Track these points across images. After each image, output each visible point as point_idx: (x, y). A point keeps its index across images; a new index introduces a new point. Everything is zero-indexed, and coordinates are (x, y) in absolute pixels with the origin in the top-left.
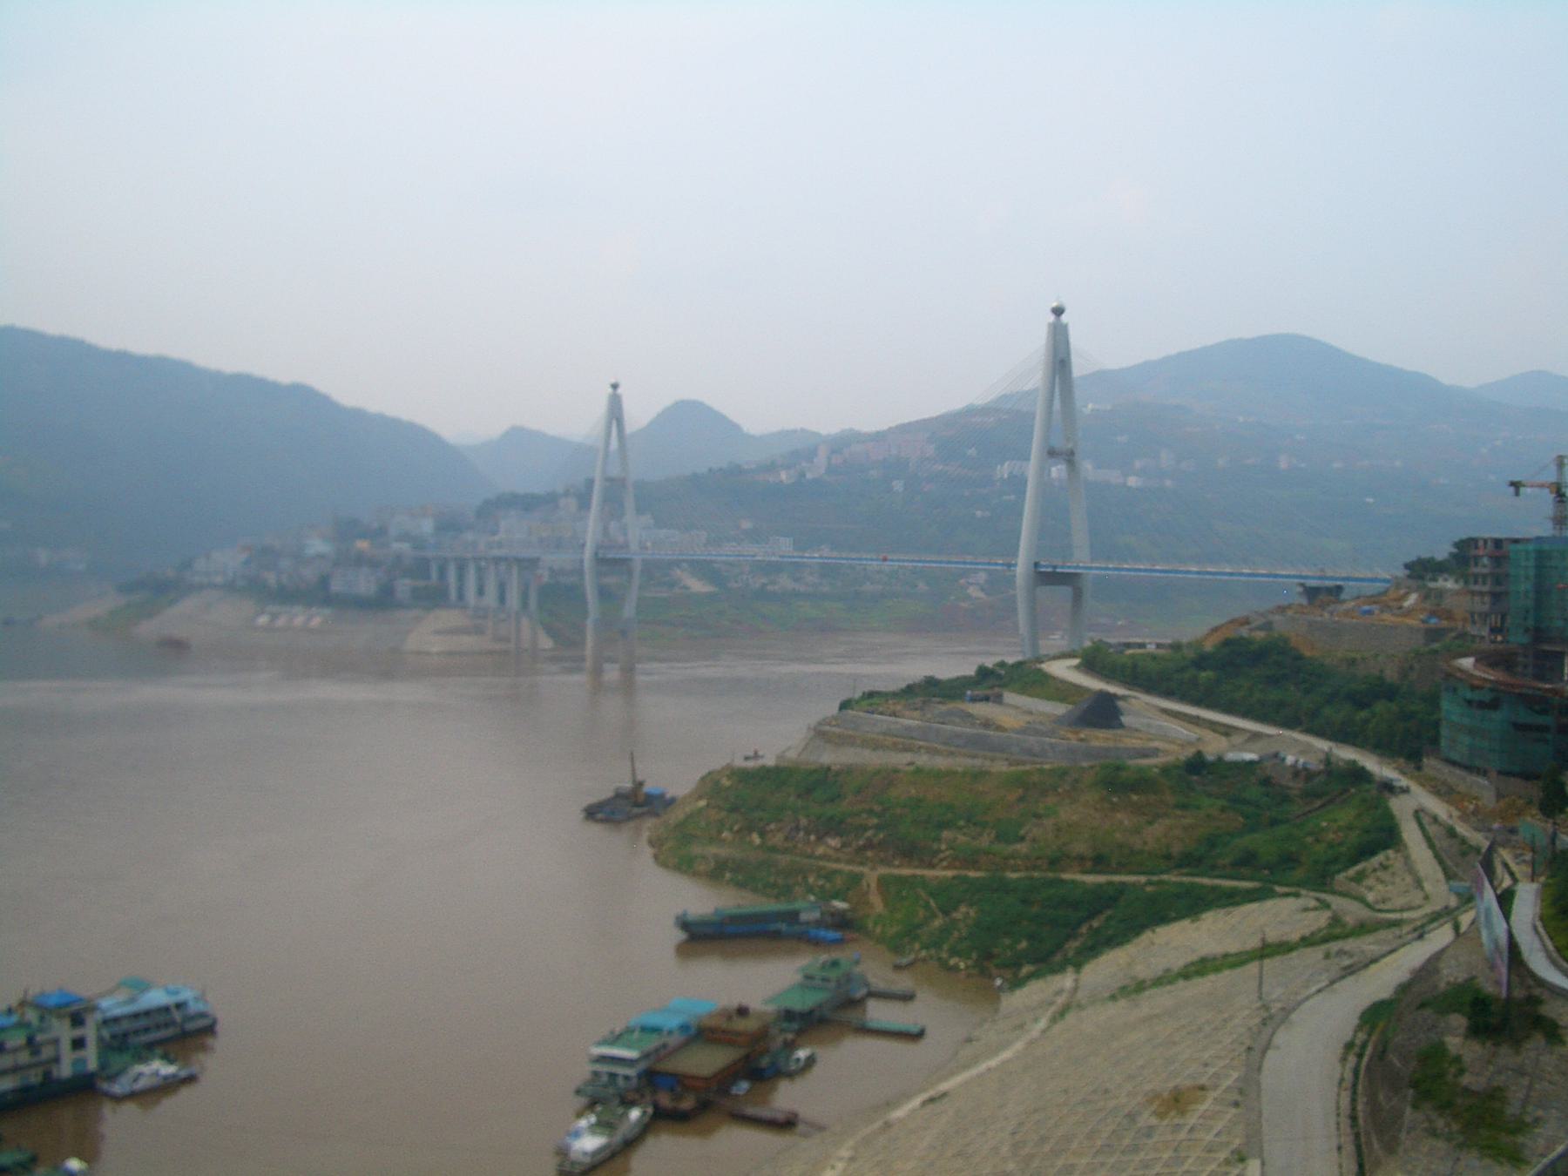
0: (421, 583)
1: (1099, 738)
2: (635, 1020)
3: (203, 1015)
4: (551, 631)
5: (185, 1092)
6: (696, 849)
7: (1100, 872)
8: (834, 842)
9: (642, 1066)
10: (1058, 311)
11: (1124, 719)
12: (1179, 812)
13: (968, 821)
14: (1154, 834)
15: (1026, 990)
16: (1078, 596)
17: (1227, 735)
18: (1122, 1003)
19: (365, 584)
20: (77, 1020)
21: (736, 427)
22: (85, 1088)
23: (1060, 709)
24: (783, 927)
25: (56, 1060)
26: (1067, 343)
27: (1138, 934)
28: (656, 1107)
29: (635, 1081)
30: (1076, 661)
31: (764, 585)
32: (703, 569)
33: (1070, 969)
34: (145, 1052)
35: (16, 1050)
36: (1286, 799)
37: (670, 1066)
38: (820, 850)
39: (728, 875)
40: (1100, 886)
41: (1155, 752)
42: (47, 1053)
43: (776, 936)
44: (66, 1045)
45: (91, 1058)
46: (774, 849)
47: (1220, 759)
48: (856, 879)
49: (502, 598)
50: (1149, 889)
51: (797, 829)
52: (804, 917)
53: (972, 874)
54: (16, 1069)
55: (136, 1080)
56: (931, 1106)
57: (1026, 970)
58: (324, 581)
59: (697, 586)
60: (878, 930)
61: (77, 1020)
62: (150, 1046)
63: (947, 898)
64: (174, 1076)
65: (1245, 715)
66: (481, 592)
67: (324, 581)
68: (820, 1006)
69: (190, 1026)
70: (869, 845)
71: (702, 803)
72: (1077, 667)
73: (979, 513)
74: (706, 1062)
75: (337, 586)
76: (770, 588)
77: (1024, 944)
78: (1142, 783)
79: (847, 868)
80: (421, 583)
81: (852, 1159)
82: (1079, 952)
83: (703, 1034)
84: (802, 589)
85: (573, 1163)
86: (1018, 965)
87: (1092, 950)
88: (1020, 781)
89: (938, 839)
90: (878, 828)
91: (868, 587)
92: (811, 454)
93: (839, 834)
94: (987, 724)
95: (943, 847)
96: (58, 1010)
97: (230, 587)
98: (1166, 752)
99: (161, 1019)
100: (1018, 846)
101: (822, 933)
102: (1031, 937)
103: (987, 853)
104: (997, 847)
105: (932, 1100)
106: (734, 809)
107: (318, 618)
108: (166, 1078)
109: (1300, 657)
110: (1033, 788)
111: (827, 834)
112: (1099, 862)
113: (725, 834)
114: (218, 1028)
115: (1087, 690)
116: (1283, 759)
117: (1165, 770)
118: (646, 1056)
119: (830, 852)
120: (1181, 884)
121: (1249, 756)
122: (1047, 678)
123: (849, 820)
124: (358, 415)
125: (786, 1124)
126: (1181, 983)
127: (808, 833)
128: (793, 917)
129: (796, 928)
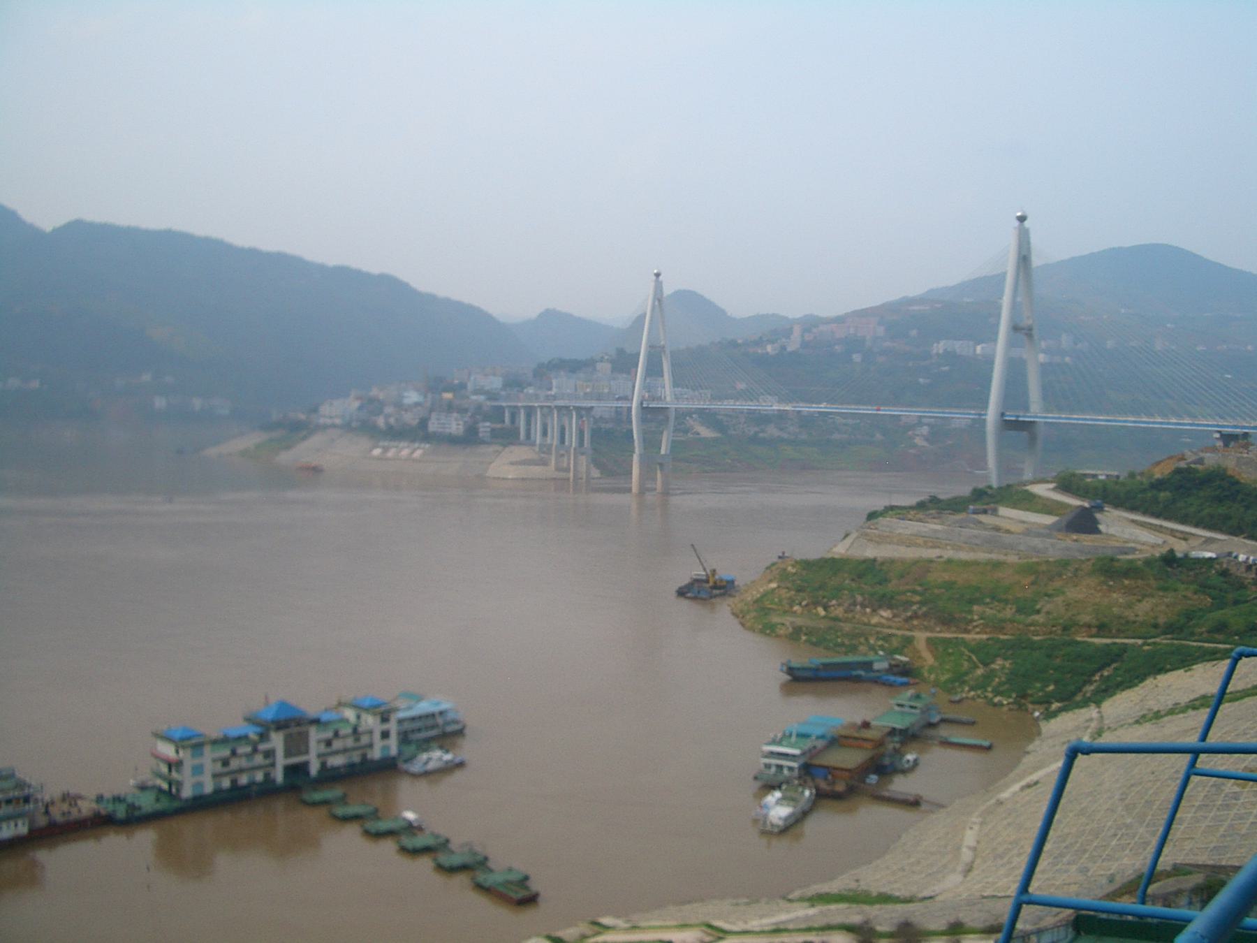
0: (499, 426)
1: (1087, 540)
2: (795, 728)
3: (456, 722)
4: (597, 463)
5: (458, 776)
6: (775, 619)
7: (1102, 637)
8: (886, 613)
9: (802, 761)
10: (1022, 219)
11: (1101, 527)
12: (1161, 593)
13: (993, 598)
14: (1144, 609)
15: (1059, 719)
16: (1033, 439)
17: (1185, 539)
18: (1148, 725)
19: (455, 426)
20: (385, 719)
21: (723, 312)
22: (389, 767)
23: (1049, 520)
24: (862, 673)
25: (371, 746)
26: (1029, 243)
27: (1142, 680)
28: (817, 789)
29: (796, 773)
30: (1052, 486)
31: (756, 433)
32: (708, 417)
33: (1093, 706)
34: (425, 744)
35: (345, 737)
36: (1242, 586)
37: (816, 762)
38: (875, 620)
39: (804, 638)
40: (1107, 645)
41: (1134, 550)
42: (365, 740)
43: (858, 679)
44: (377, 735)
45: (393, 745)
46: (836, 619)
47: (1186, 556)
48: (909, 641)
49: (562, 440)
50: (1146, 648)
51: (855, 604)
52: (876, 666)
53: (1002, 637)
54: (345, 751)
55: (426, 763)
56: (1029, 790)
57: (1055, 705)
58: (424, 423)
59: (706, 432)
60: (933, 677)
61: (385, 719)
62: (428, 741)
63: (984, 654)
64: (451, 761)
65: (1196, 526)
66: (545, 433)
67: (424, 423)
68: (913, 725)
69: (449, 729)
70: (915, 616)
71: (774, 585)
72: (1054, 489)
73: (921, 380)
74: (850, 759)
75: (433, 427)
76: (761, 435)
77: (1051, 688)
78: (1131, 571)
79: (900, 633)
80: (499, 426)
81: (982, 824)
82: (1096, 692)
83: (836, 741)
84: (786, 436)
85: (772, 825)
86: (1050, 703)
87: (1107, 690)
88: (1030, 569)
89: (970, 612)
90: (922, 603)
91: (836, 436)
92: (788, 333)
93: (890, 607)
94: (997, 529)
95: (976, 617)
96: (373, 709)
97: (348, 427)
98: (1141, 551)
99: (430, 722)
100: (1036, 617)
101: (892, 678)
102: (1056, 682)
103: (1012, 621)
104: (1020, 618)
105: (1029, 786)
106: (800, 590)
107: (419, 451)
108: (447, 762)
109: (1238, 483)
110: (1045, 574)
111: (880, 607)
112: (1102, 629)
113: (796, 608)
114: (466, 731)
115: (1067, 506)
116: (1236, 557)
117: (1148, 562)
118: (803, 754)
119: (884, 621)
120: (1172, 645)
121: (1208, 555)
122: (1032, 497)
123: (898, 597)
124: (432, 298)
125: (914, 803)
126: (1191, 712)
127: (863, 606)
128: (868, 666)
129: (872, 675)
